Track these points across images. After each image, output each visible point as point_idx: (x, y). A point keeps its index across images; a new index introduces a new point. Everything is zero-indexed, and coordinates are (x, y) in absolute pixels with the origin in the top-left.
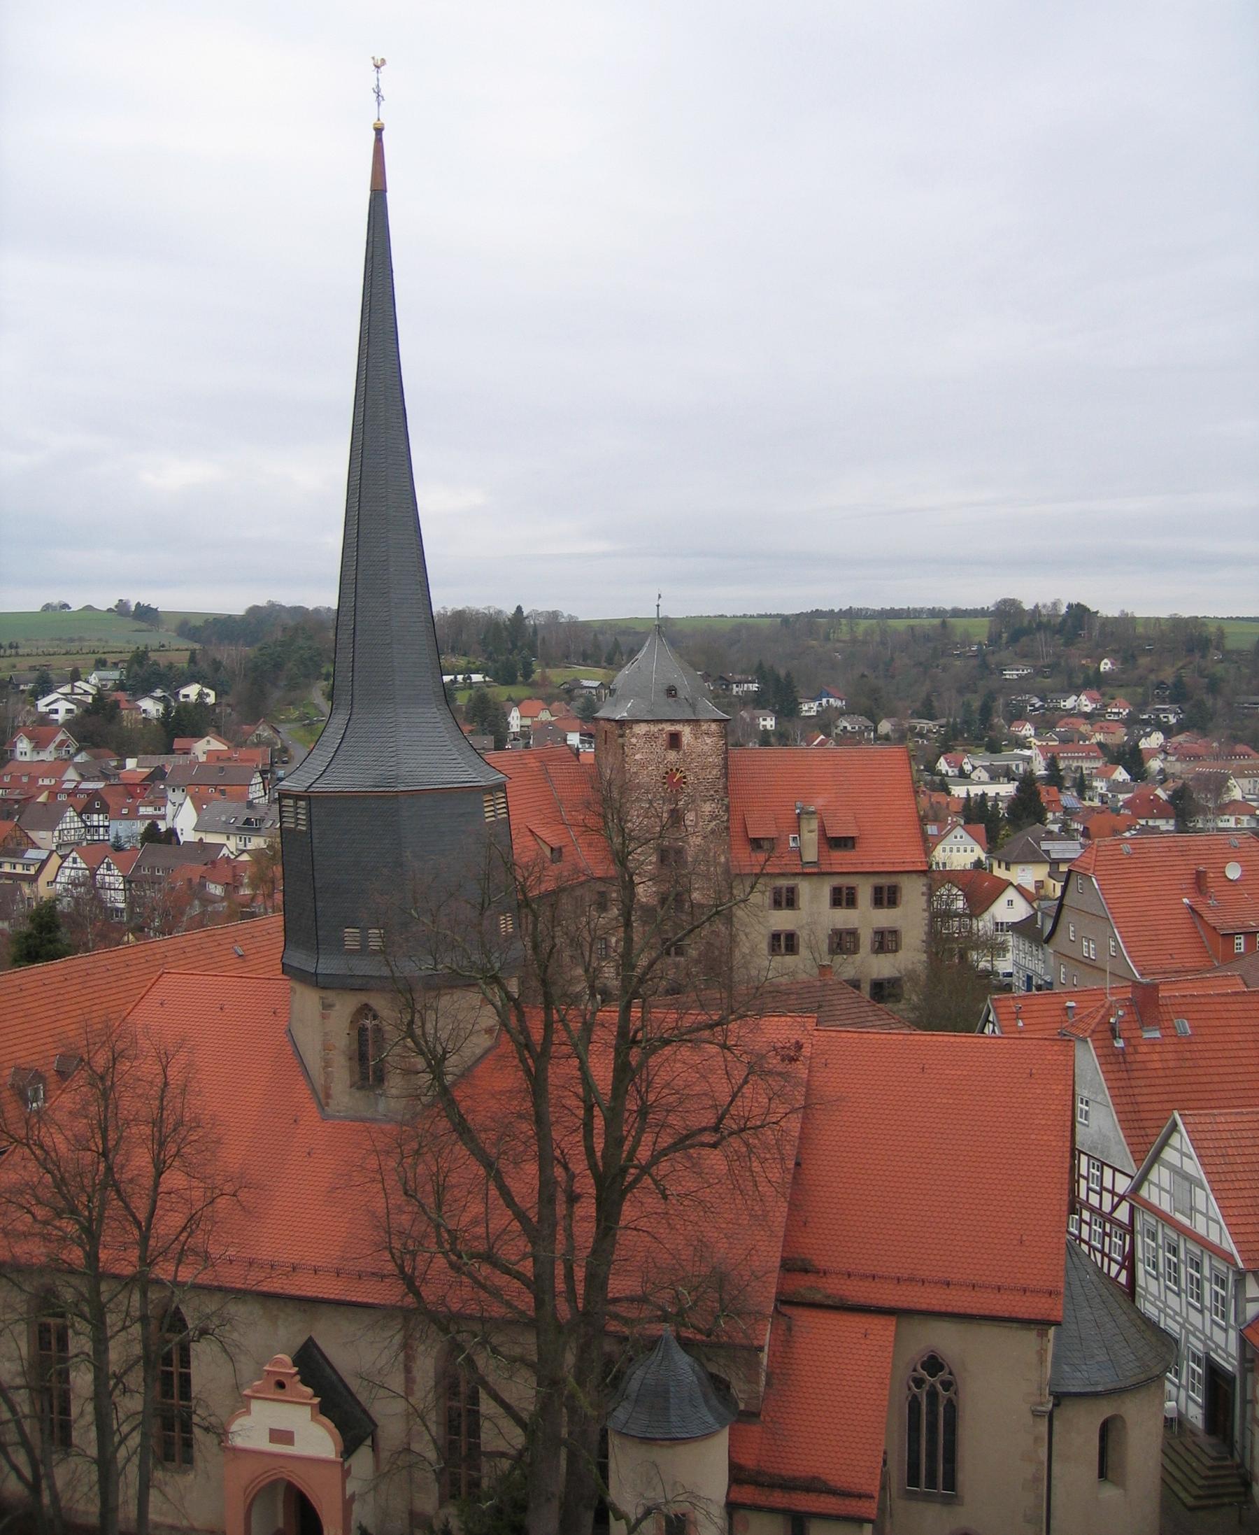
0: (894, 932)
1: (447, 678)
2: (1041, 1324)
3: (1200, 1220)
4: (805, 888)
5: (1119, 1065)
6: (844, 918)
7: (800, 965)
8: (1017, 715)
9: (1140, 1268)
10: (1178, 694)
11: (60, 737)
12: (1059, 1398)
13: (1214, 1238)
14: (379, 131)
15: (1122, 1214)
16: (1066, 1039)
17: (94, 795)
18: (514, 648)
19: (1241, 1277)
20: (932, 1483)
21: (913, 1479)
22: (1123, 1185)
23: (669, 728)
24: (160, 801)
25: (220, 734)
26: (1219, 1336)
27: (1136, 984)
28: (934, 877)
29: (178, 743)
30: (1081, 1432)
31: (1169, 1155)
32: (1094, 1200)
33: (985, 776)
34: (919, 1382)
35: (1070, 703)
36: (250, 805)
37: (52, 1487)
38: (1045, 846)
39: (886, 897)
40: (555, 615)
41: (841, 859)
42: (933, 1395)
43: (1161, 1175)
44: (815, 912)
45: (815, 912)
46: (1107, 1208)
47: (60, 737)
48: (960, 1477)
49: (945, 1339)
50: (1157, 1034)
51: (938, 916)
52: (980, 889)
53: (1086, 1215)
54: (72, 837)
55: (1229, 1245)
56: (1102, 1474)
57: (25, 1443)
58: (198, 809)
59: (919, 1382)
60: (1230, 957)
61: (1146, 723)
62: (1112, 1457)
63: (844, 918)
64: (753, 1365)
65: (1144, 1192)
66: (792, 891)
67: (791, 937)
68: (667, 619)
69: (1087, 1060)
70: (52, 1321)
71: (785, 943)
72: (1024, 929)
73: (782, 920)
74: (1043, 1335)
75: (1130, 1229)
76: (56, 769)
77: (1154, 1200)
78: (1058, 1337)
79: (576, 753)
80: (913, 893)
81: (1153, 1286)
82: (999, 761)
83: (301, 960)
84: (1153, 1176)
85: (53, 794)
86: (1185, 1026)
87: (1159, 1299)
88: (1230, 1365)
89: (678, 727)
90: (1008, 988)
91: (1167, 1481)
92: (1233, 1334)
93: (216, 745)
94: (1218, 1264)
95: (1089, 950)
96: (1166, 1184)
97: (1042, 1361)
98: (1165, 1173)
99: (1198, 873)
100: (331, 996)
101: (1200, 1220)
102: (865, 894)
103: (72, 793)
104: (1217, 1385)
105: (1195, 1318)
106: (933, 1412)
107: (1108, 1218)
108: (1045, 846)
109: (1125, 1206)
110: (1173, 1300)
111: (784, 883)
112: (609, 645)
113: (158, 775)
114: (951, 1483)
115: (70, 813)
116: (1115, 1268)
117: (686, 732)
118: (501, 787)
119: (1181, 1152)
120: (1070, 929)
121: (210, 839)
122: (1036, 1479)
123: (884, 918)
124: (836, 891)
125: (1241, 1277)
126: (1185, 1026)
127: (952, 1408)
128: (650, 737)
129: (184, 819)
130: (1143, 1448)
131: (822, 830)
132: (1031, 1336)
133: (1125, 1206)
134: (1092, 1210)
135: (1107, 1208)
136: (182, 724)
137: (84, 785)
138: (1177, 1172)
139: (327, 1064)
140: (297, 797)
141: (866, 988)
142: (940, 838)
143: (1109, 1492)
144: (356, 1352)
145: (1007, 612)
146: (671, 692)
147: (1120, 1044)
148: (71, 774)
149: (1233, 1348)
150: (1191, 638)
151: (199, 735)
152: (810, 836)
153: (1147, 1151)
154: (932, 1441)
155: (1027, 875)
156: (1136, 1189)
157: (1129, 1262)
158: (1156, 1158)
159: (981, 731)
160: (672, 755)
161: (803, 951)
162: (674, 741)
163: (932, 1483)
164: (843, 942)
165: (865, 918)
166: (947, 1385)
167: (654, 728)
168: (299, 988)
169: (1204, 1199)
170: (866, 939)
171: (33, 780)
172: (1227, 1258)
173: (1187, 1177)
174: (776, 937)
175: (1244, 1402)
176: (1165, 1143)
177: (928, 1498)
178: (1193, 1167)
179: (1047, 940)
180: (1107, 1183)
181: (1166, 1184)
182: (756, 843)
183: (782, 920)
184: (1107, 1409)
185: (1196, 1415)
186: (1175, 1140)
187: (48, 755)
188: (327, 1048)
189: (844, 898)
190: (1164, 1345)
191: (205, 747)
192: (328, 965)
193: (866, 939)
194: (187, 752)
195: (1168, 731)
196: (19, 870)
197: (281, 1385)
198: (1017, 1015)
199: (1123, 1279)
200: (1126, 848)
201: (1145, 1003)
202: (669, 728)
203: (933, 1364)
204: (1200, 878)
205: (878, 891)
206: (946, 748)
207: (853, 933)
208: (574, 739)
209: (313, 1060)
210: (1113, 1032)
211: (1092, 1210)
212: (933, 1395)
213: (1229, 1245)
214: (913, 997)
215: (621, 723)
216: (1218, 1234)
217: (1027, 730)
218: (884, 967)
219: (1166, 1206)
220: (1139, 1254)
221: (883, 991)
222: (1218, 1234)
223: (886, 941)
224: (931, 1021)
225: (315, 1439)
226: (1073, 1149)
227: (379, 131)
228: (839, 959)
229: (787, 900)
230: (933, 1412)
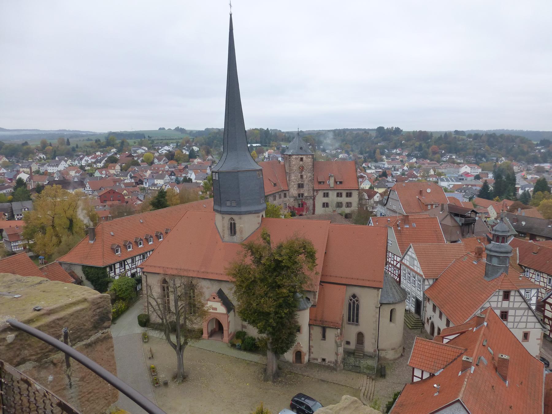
0: (351, 203)
1: (249, 145)
2: (378, 289)
3: (416, 267)
4: (330, 193)
5: (399, 233)
6: (340, 199)
7: (329, 210)
8: (382, 153)
9: (402, 277)
10: (420, 148)
11: (164, 159)
12: (382, 304)
13: (418, 271)
14: (231, 15)
15: (398, 266)
16: (386, 227)
17: (172, 172)
18: (267, 137)
19: (424, 280)
20: (353, 321)
21: (349, 320)
22: (399, 259)
23: (300, 156)
24: (187, 173)
25: (200, 158)
26: (419, 293)
27: (404, 215)
28: (361, 192)
29: (191, 160)
30: (386, 311)
31: (409, 253)
32: (392, 262)
33: (373, 168)
34: (351, 300)
35: (394, 151)
36: (207, 174)
37: (166, 319)
38: (387, 184)
39: (349, 195)
40: (276, 130)
41: (340, 187)
42: (354, 303)
43: (407, 257)
44: (333, 198)
45: (333, 198)
46: (395, 264)
47: (164, 159)
48: (359, 320)
49: (357, 291)
50: (476, 263)
51: (361, 198)
52: (371, 193)
53: (390, 266)
54: (168, 181)
55: (422, 273)
56: (391, 321)
57: (160, 310)
58: (196, 175)
59: (351, 300)
60: (427, 210)
61: (413, 156)
62: (393, 318)
63: (340, 199)
64: (315, 295)
65: (403, 261)
66: (327, 193)
67: (327, 204)
68: (301, 131)
69: (392, 233)
70: (165, 285)
71: (326, 205)
72: (380, 203)
73: (325, 200)
74: (378, 290)
75: (400, 269)
76: (163, 166)
77: (405, 263)
78: (382, 291)
79: (280, 162)
80: (355, 194)
81: (405, 281)
82: (377, 164)
83: (217, 208)
84: (405, 258)
85: (163, 172)
86: (414, 225)
87: (405, 284)
88: (421, 299)
89: (303, 156)
90: (376, 215)
91: (405, 322)
92: (422, 292)
93: (199, 160)
94: (413, 273)
95: (394, 207)
96: (408, 259)
97: (378, 296)
98: (408, 257)
99: (421, 191)
100: (224, 216)
101: (416, 267)
102: (344, 194)
103: (167, 171)
104: (418, 304)
105: (414, 288)
106: (354, 306)
107: (395, 266)
108: (387, 184)
109: (399, 264)
110: (409, 285)
111: (326, 192)
112: (288, 137)
113: (186, 167)
114: (357, 321)
115: (167, 176)
116: (396, 277)
117: (304, 157)
118: (261, 170)
119: (411, 252)
120: (390, 202)
121: (198, 181)
122: (376, 321)
123: (348, 200)
124: (338, 194)
125: (424, 280)
126: (414, 225)
127: (358, 306)
128: (296, 159)
129: (193, 176)
130: (400, 315)
131: (335, 180)
132: (376, 291)
133: (399, 264)
134: (392, 264)
135: (395, 264)
136: (193, 155)
137: (170, 169)
138: (411, 257)
139: (223, 230)
140: (216, 172)
141: (344, 216)
142: (361, 182)
143: (392, 325)
144: (230, 292)
145: (380, 129)
146: (301, 148)
147: (399, 228)
148: (167, 167)
149: (422, 295)
150: (423, 136)
151: (195, 158)
152: (332, 181)
153: (404, 253)
154: (353, 313)
155: (381, 190)
156: (401, 260)
157: (399, 276)
158: (406, 253)
159: (373, 157)
160: (301, 163)
161: (330, 207)
162: (302, 159)
163: (353, 321)
164: (339, 205)
165: (344, 199)
166: (357, 301)
167: (297, 157)
168: (216, 213)
169: (416, 263)
170: (344, 205)
171: (158, 168)
172: (421, 276)
173: (413, 258)
174: (324, 204)
175: (424, 307)
176: (408, 250)
177: (352, 324)
178: (414, 256)
179: (385, 205)
180: (395, 259)
181: (408, 259)
182: (320, 183)
183: (325, 200)
184: (392, 307)
185: (413, 309)
186: (411, 250)
187: (162, 163)
188: (223, 227)
189: (339, 195)
190: (404, 294)
191: (197, 161)
192: (224, 209)
193: (344, 205)
194: (193, 162)
195: (417, 158)
196: (156, 188)
197: (214, 298)
198: (377, 222)
199: (398, 280)
200: (404, 185)
201: (406, 219)
202: (300, 156)
203: (354, 296)
204: (421, 192)
205: (347, 193)
206: (365, 161)
207: (341, 203)
208: (280, 159)
209: (220, 230)
210: (398, 226)
211: (392, 264)
212: (354, 303)
213: (422, 273)
214: (354, 217)
215: (290, 155)
216: (419, 270)
217: (384, 157)
218: (348, 210)
219: (408, 264)
220: (402, 274)
221: (347, 216)
222: (419, 270)
223: (349, 205)
224: (357, 222)
225: (221, 309)
226: (387, 251)
227: (231, 15)
228: (338, 209)
229: (326, 195)
230: (354, 306)
